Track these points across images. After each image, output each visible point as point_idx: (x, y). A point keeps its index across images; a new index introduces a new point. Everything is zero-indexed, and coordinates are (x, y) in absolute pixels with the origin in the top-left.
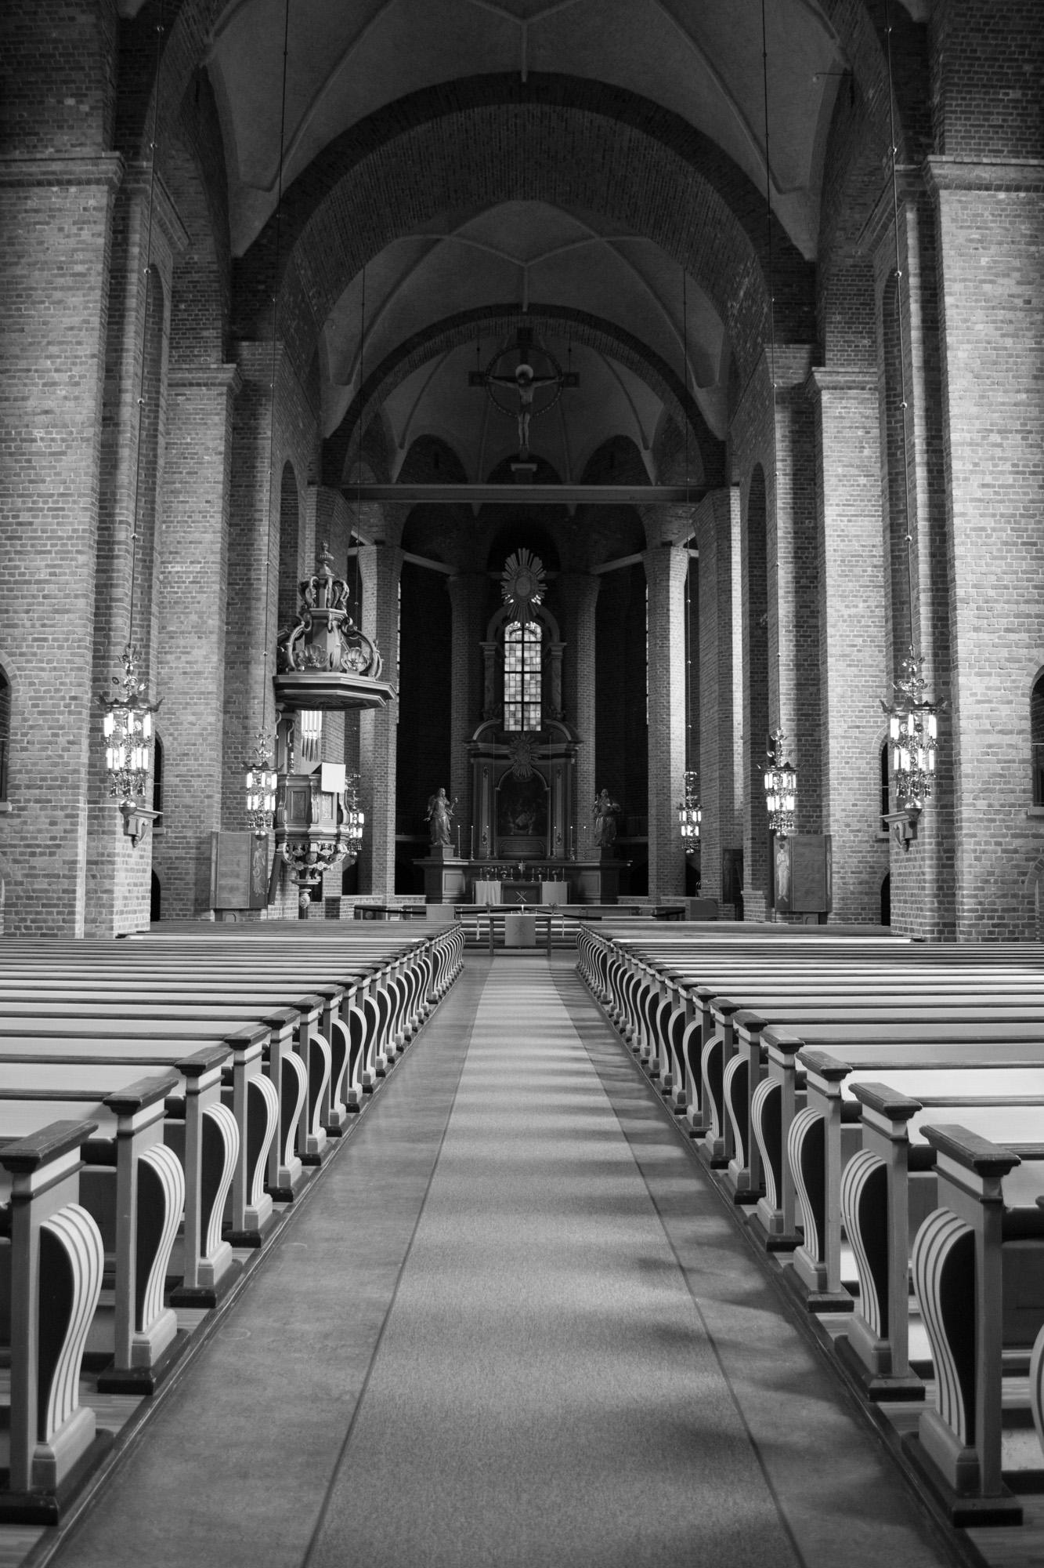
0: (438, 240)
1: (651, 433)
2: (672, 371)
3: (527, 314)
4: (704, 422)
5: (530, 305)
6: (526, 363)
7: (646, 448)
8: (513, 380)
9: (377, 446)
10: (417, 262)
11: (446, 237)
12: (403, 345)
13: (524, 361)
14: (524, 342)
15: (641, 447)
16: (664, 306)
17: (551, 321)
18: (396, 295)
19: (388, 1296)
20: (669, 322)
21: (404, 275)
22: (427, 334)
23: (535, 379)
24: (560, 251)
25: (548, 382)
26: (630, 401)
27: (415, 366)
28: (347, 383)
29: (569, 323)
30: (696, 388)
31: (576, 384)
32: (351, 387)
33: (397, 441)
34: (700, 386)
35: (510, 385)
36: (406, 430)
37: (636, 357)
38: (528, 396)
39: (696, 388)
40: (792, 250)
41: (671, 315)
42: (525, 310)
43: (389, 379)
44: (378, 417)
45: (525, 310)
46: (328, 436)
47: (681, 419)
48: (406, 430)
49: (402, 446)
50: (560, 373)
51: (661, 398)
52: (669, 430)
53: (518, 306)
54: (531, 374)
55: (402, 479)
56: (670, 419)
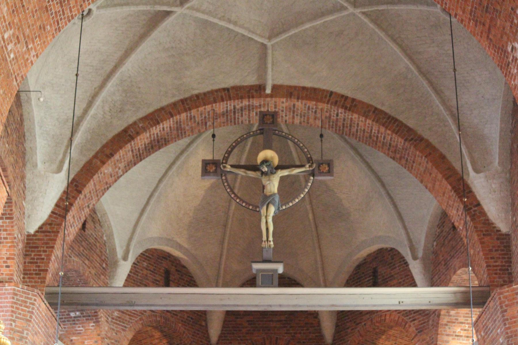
0: (168, 13)
1: (421, 235)
2: (443, 157)
3: (271, 96)
4: (483, 213)
5: (275, 88)
6: (270, 148)
7: (415, 258)
8: (255, 168)
9: (92, 242)
10: (143, 37)
11: (178, 10)
12: (125, 131)
13: (268, 146)
14: (268, 128)
15: (409, 258)
16: (431, 83)
17: (299, 104)
18: (117, 75)
19: (31, 90)
20: (437, 101)
21: (127, 54)
22: (153, 119)
23: (280, 167)
24: (308, 26)
25: (296, 171)
26: (395, 206)
27: (139, 157)
28: (59, 170)
29: (320, 106)
30: (472, 173)
31: (330, 172)
32: (63, 174)
33: (120, 252)
34: (477, 171)
35: (251, 174)
36: (130, 239)
37: (399, 141)
38: (273, 185)
39: (472, 173)
40: (488, 223)
41: (438, 92)
42: (268, 91)
43: (107, 169)
44: (93, 221)
45: (268, 91)
46: (32, 231)
47: (457, 215)
48: (130, 239)
49: (125, 258)
50: (310, 160)
51: (432, 190)
52: (443, 224)
53: (260, 89)
54: (276, 161)
55: (132, 280)
56: (444, 216)
